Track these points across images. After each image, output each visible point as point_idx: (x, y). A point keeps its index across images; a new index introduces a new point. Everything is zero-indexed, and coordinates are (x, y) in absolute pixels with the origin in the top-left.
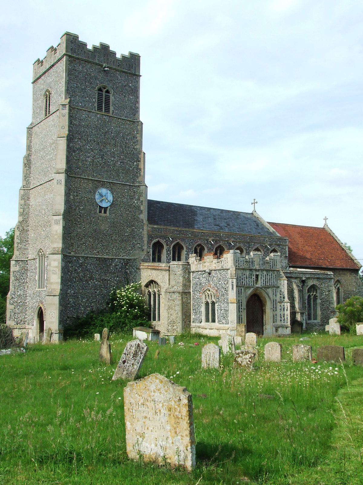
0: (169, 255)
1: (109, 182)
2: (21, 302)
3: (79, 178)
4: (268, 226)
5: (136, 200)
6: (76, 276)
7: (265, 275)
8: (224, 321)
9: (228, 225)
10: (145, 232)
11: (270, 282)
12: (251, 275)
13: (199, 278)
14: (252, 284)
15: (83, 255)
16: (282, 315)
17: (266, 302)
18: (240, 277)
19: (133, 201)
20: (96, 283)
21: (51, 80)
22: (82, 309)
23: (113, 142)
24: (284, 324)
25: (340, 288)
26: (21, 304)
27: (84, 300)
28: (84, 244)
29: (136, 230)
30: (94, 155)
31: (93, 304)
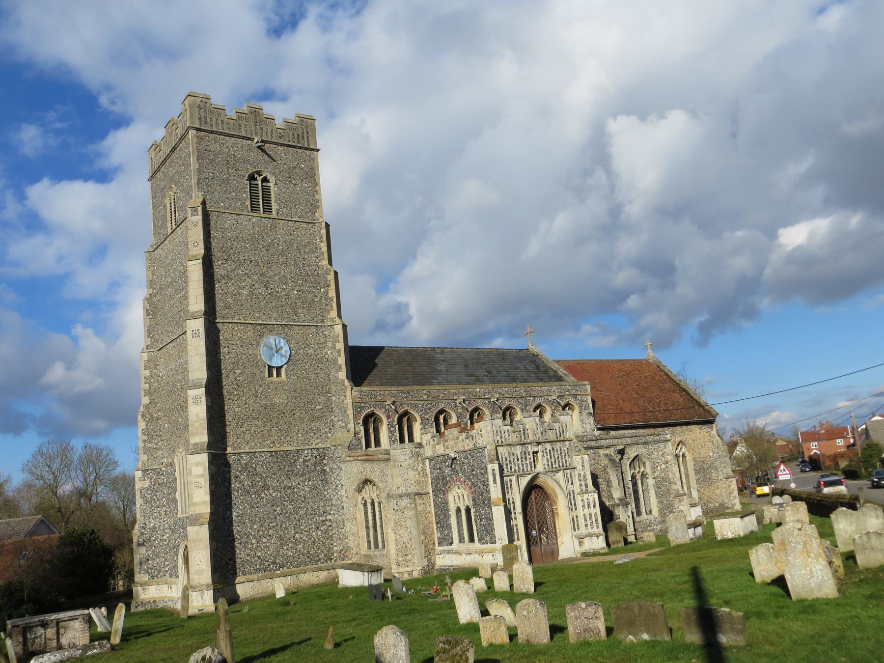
0: (393, 434)
1: (281, 325)
2: (156, 539)
3: (230, 323)
4: (555, 366)
5: (329, 350)
6: (239, 488)
7: (550, 451)
8: (488, 539)
9: (489, 373)
10: (349, 401)
11: (559, 462)
12: (525, 453)
13: (440, 469)
14: (529, 469)
15: (247, 450)
16: (587, 515)
17: (556, 496)
18: (506, 460)
19: (325, 351)
20: (274, 494)
21: (174, 172)
22: (254, 541)
23: (281, 259)
24: (592, 531)
25: (687, 454)
26: (157, 542)
27: (255, 527)
28: (248, 432)
29: (334, 398)
30: (253, 283)
31: (271, 532)
